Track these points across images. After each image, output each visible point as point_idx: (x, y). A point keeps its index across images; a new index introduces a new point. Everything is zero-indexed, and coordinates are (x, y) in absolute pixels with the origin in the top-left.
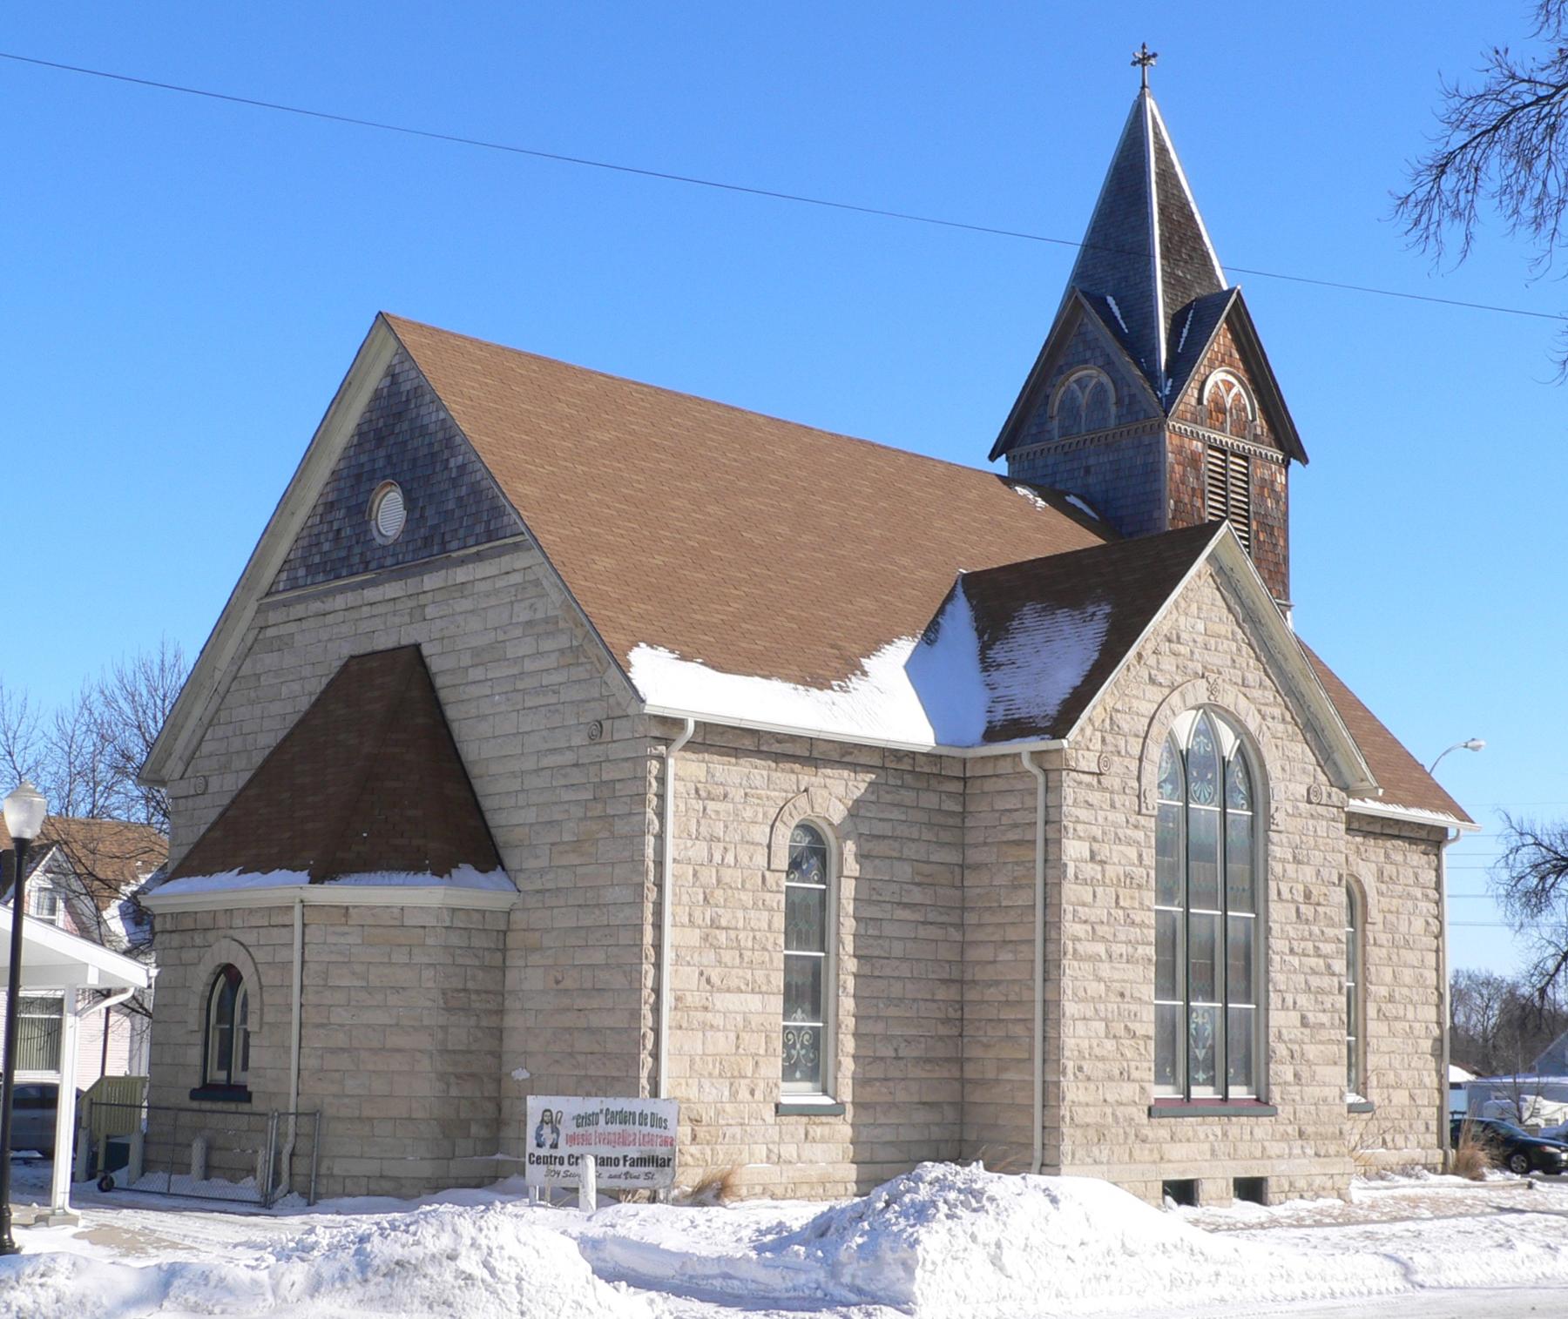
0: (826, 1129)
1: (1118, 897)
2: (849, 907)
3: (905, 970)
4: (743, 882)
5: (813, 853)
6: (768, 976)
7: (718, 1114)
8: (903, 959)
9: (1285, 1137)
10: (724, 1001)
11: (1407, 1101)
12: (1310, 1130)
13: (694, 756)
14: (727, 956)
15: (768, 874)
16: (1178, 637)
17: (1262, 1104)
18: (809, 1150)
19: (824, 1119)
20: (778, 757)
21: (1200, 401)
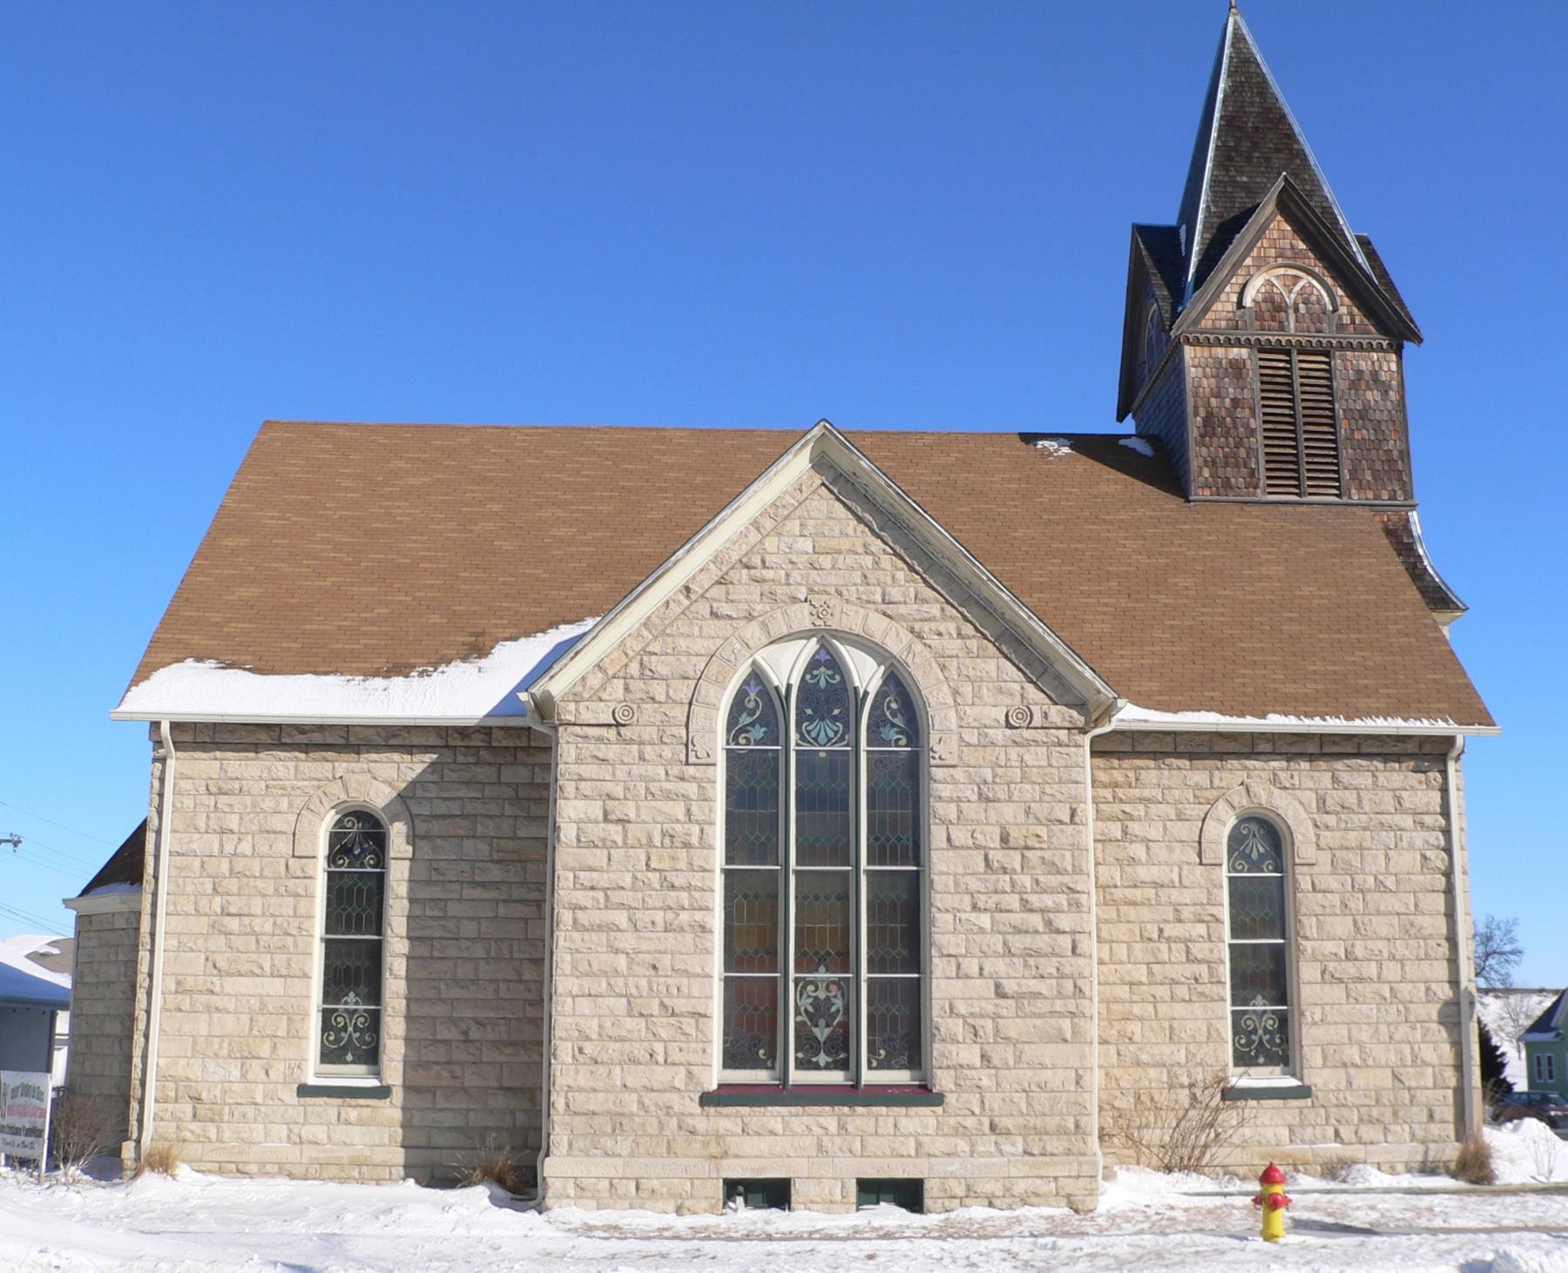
0: (366, 1112)
1: (649, 858)
2: (402, 889)
3: (479, 951)
4: (262, 870)
5: (359, 838)
6: (289, 960)
7: (224, 1092)
8: (473, 940)
9: (960, 1131)
10: (231, 984)
11: (1389, 1082)
12: (1005, 1123)
13: (204, 755)
14: (239, 942)
15: (292, 861)
16: (763, 562)
17: (924, 1094)
18: (340, 1132)
19: (362, 1102)
20: (306, 748)
21: (1240, 304)
